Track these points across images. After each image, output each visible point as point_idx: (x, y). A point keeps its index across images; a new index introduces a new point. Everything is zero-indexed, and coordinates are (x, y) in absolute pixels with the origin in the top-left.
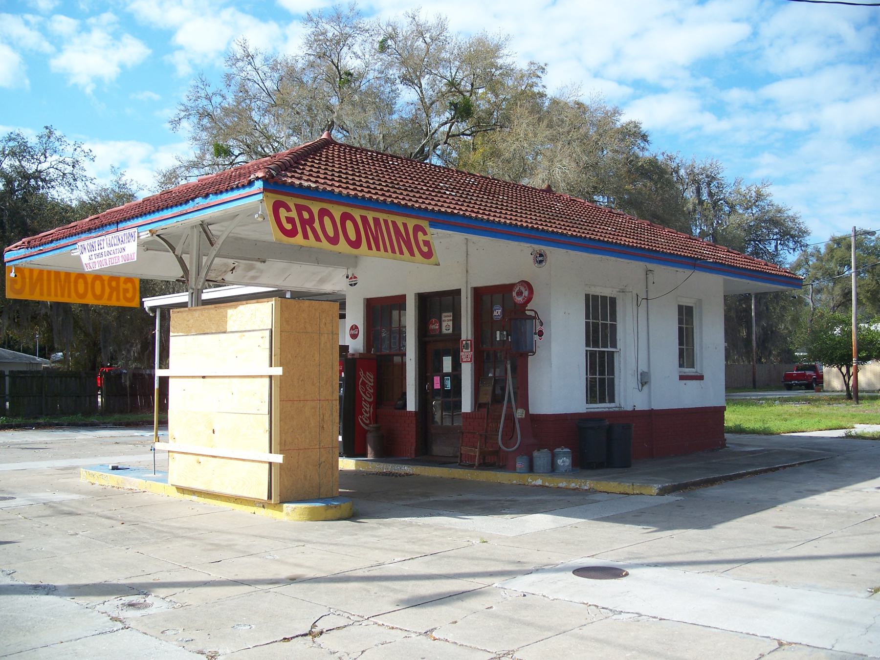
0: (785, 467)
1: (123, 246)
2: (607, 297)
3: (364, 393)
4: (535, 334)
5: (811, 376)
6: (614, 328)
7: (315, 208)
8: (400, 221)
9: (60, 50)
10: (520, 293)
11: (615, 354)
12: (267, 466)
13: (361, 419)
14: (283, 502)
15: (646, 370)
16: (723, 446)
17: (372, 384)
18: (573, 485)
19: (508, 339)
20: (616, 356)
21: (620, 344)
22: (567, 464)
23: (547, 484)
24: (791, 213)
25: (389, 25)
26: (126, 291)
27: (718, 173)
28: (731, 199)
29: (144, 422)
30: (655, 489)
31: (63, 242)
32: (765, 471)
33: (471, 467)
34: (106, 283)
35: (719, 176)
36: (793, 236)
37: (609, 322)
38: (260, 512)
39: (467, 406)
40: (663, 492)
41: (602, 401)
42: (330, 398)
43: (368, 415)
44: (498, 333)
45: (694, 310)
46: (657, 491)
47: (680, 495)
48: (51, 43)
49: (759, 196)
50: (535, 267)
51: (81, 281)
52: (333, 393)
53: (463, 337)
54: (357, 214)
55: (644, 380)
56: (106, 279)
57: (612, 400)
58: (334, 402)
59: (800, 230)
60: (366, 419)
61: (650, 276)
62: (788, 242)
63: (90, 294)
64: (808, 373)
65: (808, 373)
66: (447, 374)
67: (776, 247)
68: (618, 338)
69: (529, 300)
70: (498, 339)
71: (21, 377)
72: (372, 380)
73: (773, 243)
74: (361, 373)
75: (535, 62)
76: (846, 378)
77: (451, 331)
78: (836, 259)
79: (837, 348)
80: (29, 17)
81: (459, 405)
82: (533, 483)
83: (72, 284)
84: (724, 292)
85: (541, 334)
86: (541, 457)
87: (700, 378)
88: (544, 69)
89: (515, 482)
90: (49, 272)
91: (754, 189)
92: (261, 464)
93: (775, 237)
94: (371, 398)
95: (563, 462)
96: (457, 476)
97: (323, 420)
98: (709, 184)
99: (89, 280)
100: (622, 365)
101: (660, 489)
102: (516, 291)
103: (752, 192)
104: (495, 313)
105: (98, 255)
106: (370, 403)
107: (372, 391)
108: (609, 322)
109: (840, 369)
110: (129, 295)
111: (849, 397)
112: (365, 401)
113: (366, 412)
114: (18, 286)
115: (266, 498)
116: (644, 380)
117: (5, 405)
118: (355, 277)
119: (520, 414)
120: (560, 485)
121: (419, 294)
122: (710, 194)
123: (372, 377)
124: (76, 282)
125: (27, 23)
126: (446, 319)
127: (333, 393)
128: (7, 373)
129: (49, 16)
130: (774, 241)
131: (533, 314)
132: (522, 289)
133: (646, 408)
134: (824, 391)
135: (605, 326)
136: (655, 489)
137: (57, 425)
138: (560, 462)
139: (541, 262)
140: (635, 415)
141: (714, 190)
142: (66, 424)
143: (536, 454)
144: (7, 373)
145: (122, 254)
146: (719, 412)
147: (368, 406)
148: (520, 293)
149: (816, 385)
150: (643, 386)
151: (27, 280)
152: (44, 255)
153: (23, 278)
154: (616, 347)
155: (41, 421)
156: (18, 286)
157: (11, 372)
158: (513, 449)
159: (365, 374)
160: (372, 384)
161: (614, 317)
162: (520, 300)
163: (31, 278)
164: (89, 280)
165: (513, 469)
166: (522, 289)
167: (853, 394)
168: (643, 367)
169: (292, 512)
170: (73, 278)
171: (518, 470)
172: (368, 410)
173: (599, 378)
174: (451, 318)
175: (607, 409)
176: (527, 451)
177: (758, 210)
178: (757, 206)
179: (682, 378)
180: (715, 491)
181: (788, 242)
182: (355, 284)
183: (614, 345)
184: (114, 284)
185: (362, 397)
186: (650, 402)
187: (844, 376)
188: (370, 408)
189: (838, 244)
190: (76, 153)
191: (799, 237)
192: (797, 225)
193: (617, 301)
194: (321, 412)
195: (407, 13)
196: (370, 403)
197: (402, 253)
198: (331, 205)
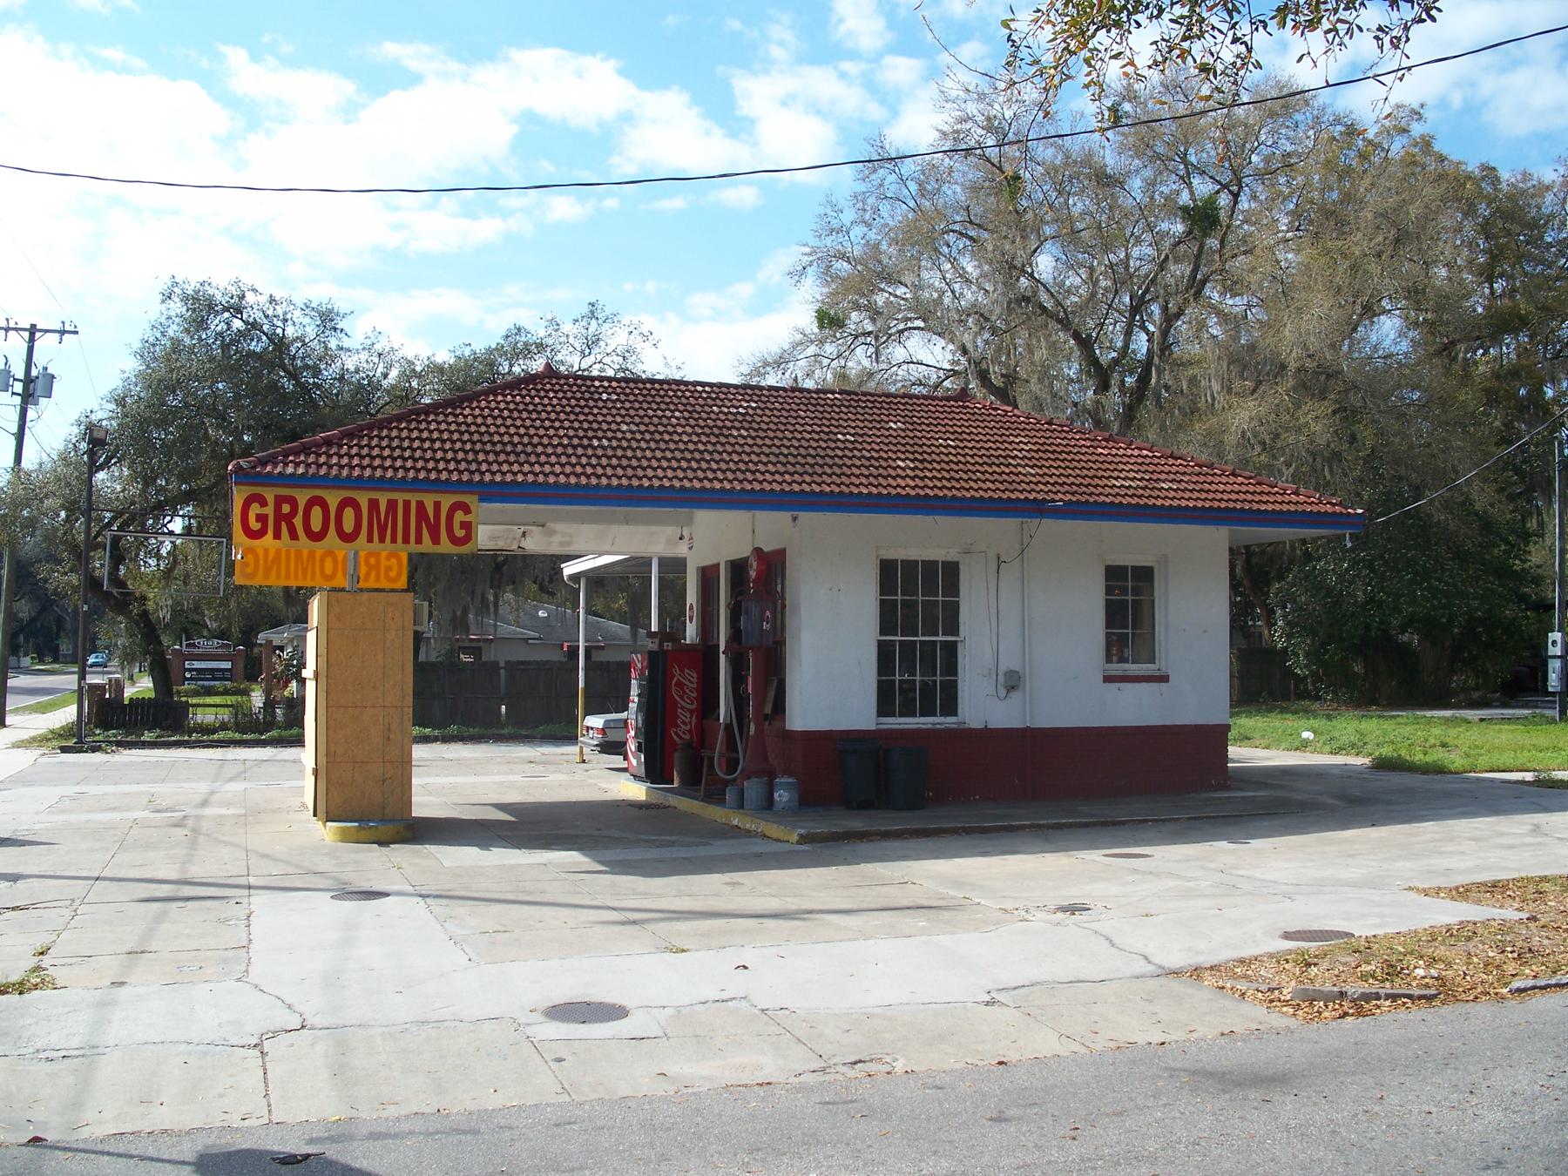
2: (937, 562)
3: (682, 698)
7: (302, 497)
9: (895, 113)
11: (959, 645)
13: (676, 734)
17: (695, 685)
21: (964, 629)
22: (784, 800)
26: (389, 569)
37: (940, 598)
40: (803, 839)
41: (928, 711)
42: (400, 704)
43: (688, 728)
45: (1156, 571)
48: (882, 102)
52: (403, 698)
54: (363, 499)
55: (1013, 683)
58: (406, 709)
60: (684, 733)
63: (340, 573)
72: (695, 680)
74: (676, 671)
80: (847, 66)
83: (317, 564)
84: (1230, 541)
87: (1164, 679)
88: (1419, 113)
94: (693, 703)
95: (780, 796)
97: (389, 729)
106: (692, 712)
107: (695, 695)
108: (940, 598)
110: (393, 574)
112: (682, 708)
113: (684, 723)
114: (249, 570)
117: (500, 708)
123: (695, 675)
124: (322, 561)
125: (843, 76)
127: (403, 698)
128: (502, 664)
129: (876, 59)
137: (527, 737)
140: (988, 736)
144: (502, 664)
146: (1216, 737)
147: (688, 715)
151: (262, 562)
153: (257, 560)
155: (505, 731)
156: (249, 570)
157: (508, 663)
159: (682, 671)
160: (695, 685)
163: (266, 559)
168: (1009, 662)
172: (687, 720)
173: (941, 681)
175: (930, 726)
179: (1108, 679)
183: (956, 632)
185: (678, 703)
188: (691, 718)
190: (632, 337)
193: (961, 567)
194: (386, 720)
196: (692, 712)
197: (394, 540)
198: (328, 491)
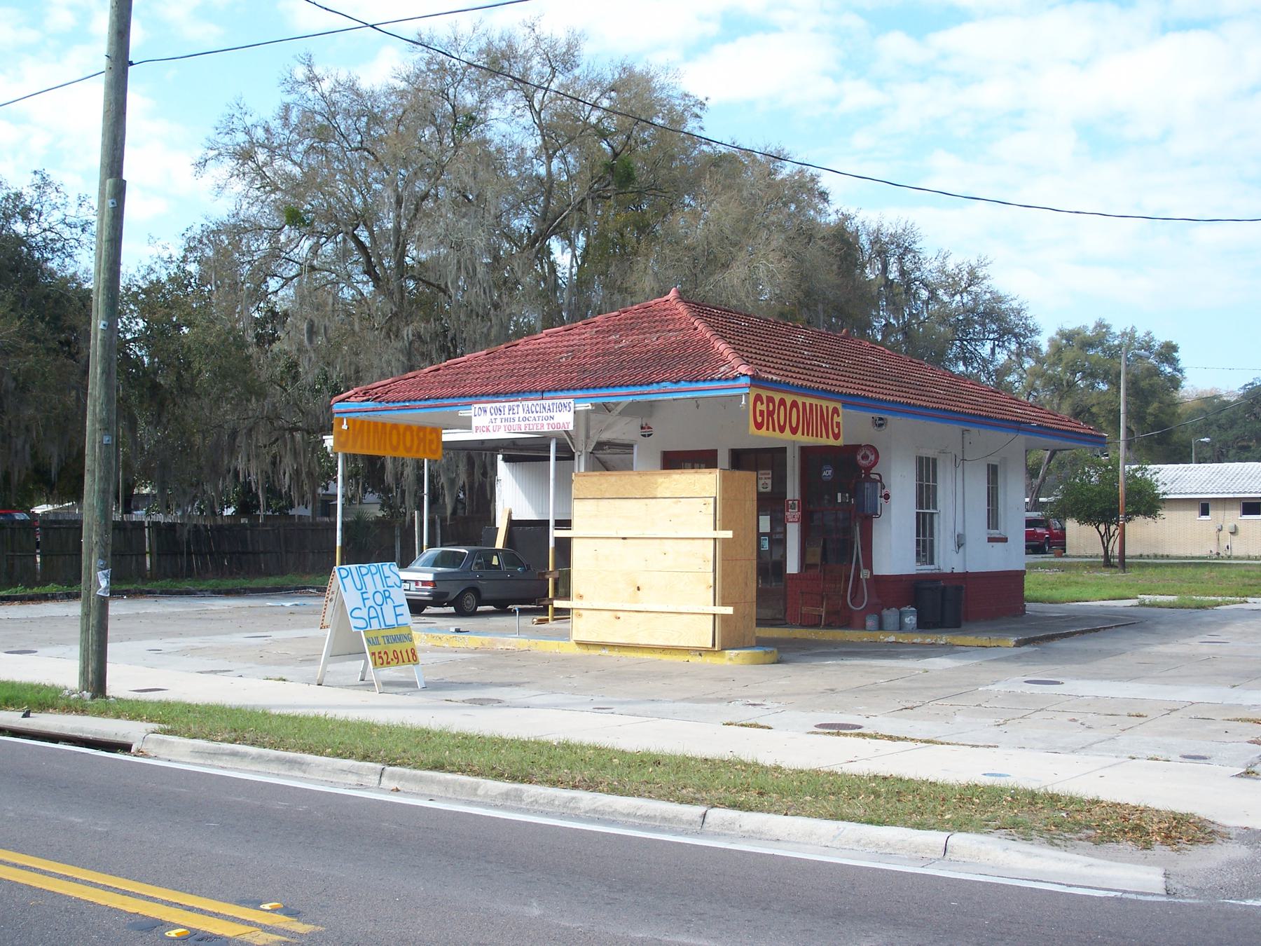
0: (1105, 628)
1: (552, 414)
4: (881, 497)
5: (1043, 535)
6: (935, 488)
8: (824, 404)
10: (865, 457)
12: (712, 617)
14: (723, 649)
15: (961, 533)
16: (1024, 611)
18: (928, 640)
19: (850, 501)
20: (936, 517)
23: (901, 640)
24: (1015, 304)
25: (502, 39)
27: (914, 242)
28: (932, 278)
29: (245, 589)
30: (1012, 641)
31: (446, 402)
32: (1090, 631)
33: (815, 625)
34: (415, 433)
35: (915, 247)
36: (1016, 336)
38: (708, 660)
39: (792, 567)
40: (1019, 644)
44: (839, 495)
46: (1014, 643)
47: (1034, 646)
49: (973, 278)
50: (874, 431)
51: (394, 432)
53: (789, 497)
55: (960, 543)
56: (415, 429)
57: (932, 563)
59: (1026, 327)
61: (966, 435)
62: (1010, 343)
64: (1039, 530)
65: (1039, 530)
66: (764, 534)
67: (993, 350)
68: (938, 500)
69: (875, 463)
70: (839, 501)
71: (55, 528)
73: (989, 345)
75: (690, 94)
76: (1105, 538)
77: (769, 489)
78: (1067, 363)
79: (1096, 501)
81: (782, 564)
82: (886, 640)
83: (388, 436)
85: (887, 497)
86: (890, 615)
87: (1005, 540)
89: (865, 639)
90: (369, 422)
91: (966, 268)
92: (704, 616)
93: (992, 336)
96: (798, 636)
98: (901, 259)
99: (402, 431)
100: (942, 527)
101: (1016, 642)
102: (861, 454)
103: (964, 273)
104: (825, 474)
105: (506, 420)
109: (1097, 528)
111: (1107, 563)
115: (711, 646)
116: (960, 543)
118: (649, 428)
119: (865, 574)
120: (915, 641)
121: (732, 450)
122: (903, 273)
126: (763, 477)
130: (988, 341)
131: (877, 477)
132: (868, 453)
133: (961, 571)
134: (1067, 556)
135: (928, 486)
136: (1012, 641)
138: (907, 620)
139: (880, 425)
141: (908, 266)
142: (158, 592)
143: (885, 612)
145: (548, 421)
148: (865, 457)
149: (1050, 547)
150: (959, 547)
152: (409, 412)
154: (936, 509)
158: (863, 607)
161: (935, 480)
162: (864, 463)
164: (402, 431)
165: (863, 627)
166: (868, 453)
167: (1115, 562)
168: (959, 530)
169: (733, 657)
170: (388, 429)
171: (868, 628)
174: (770, 476)
176: (876, 610)
177: (970, 298)
178: (970, 293)
179: (991, 540)
180: (1058, 644)
181: (1010, 343)
182: (649, 435)
184: (421, 434)
186: (965, 565)
187: (1102, 537)
189: (1068, 340)
191: (1025, 337)
192: (1023, 320)
195: (524, 21)
